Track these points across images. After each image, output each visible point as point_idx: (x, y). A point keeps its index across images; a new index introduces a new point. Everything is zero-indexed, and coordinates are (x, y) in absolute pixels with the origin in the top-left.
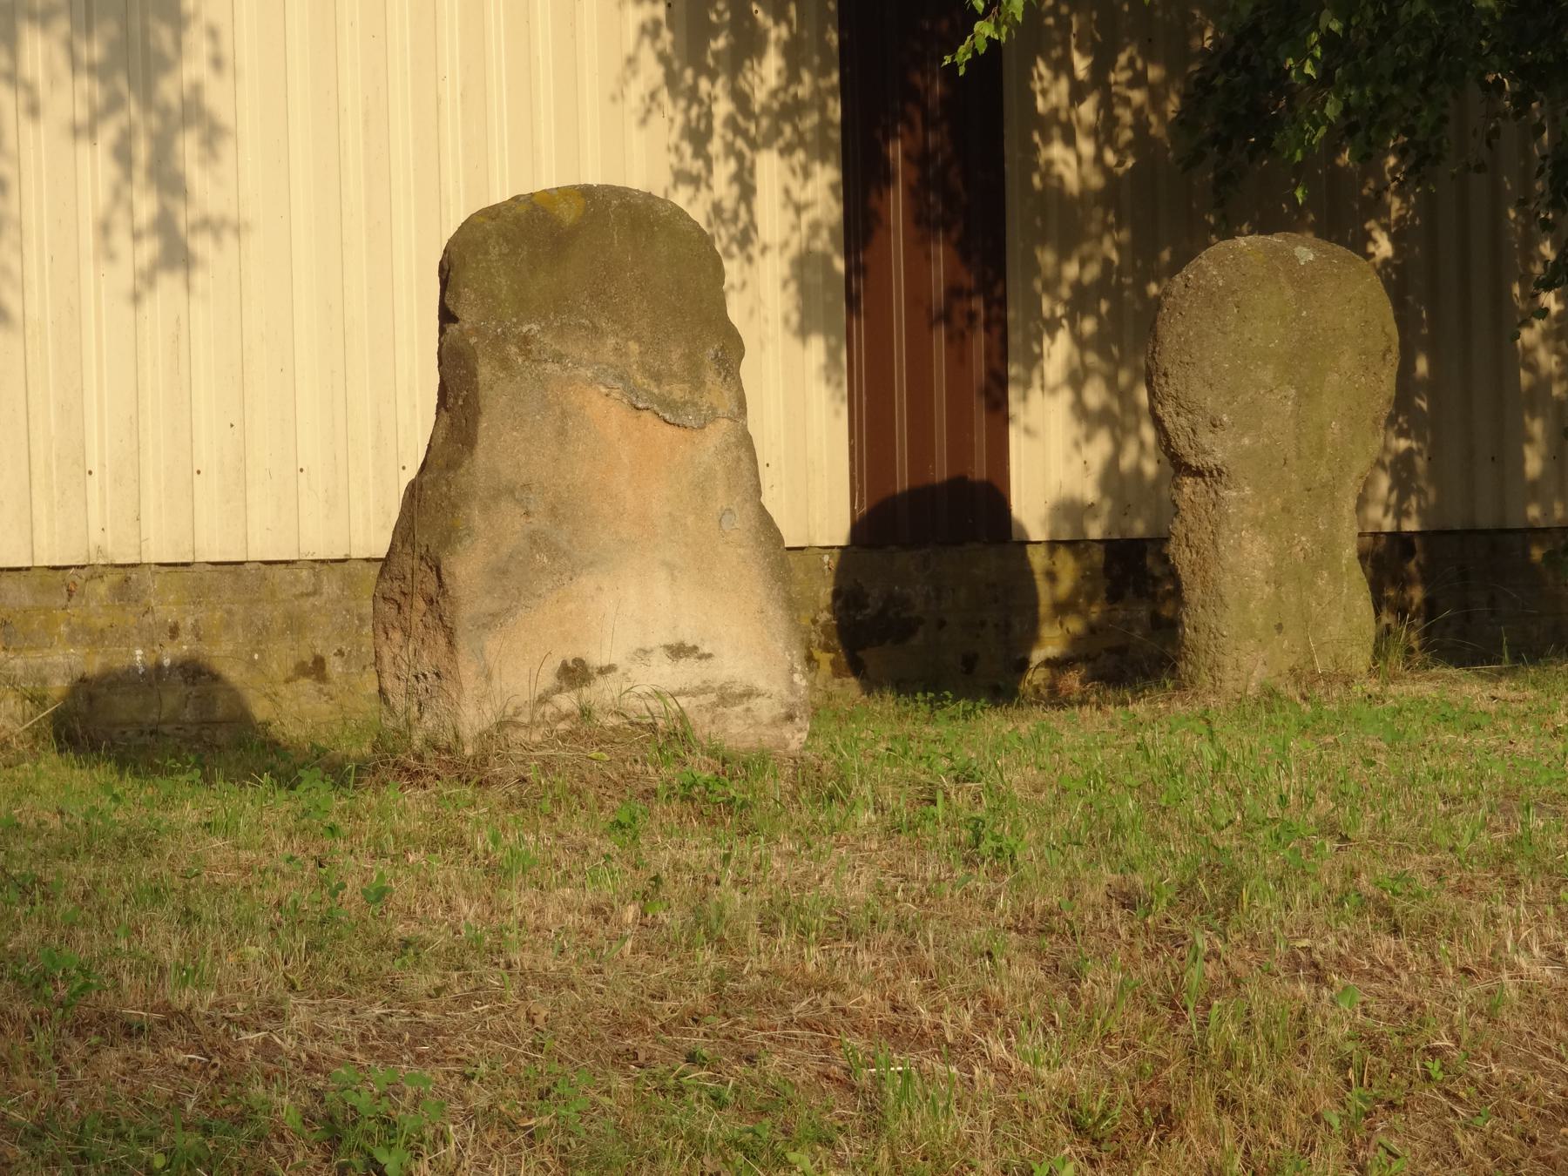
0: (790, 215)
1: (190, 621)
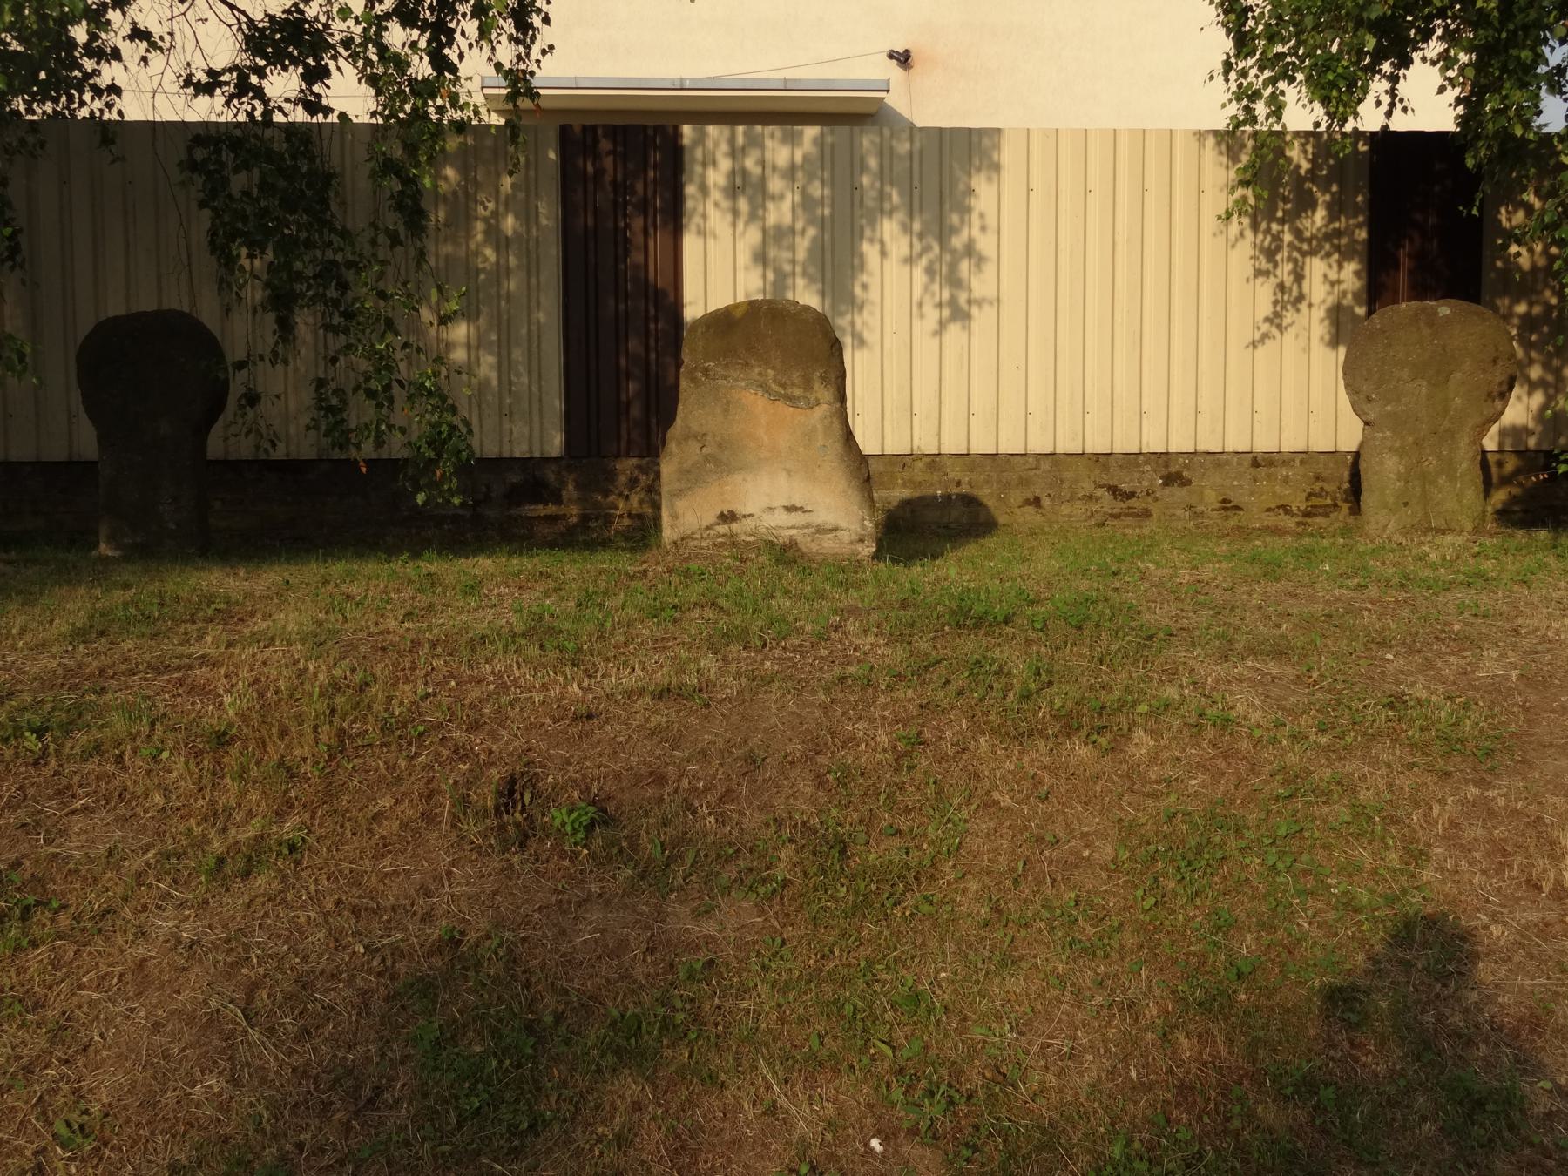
0: (1328, 287)
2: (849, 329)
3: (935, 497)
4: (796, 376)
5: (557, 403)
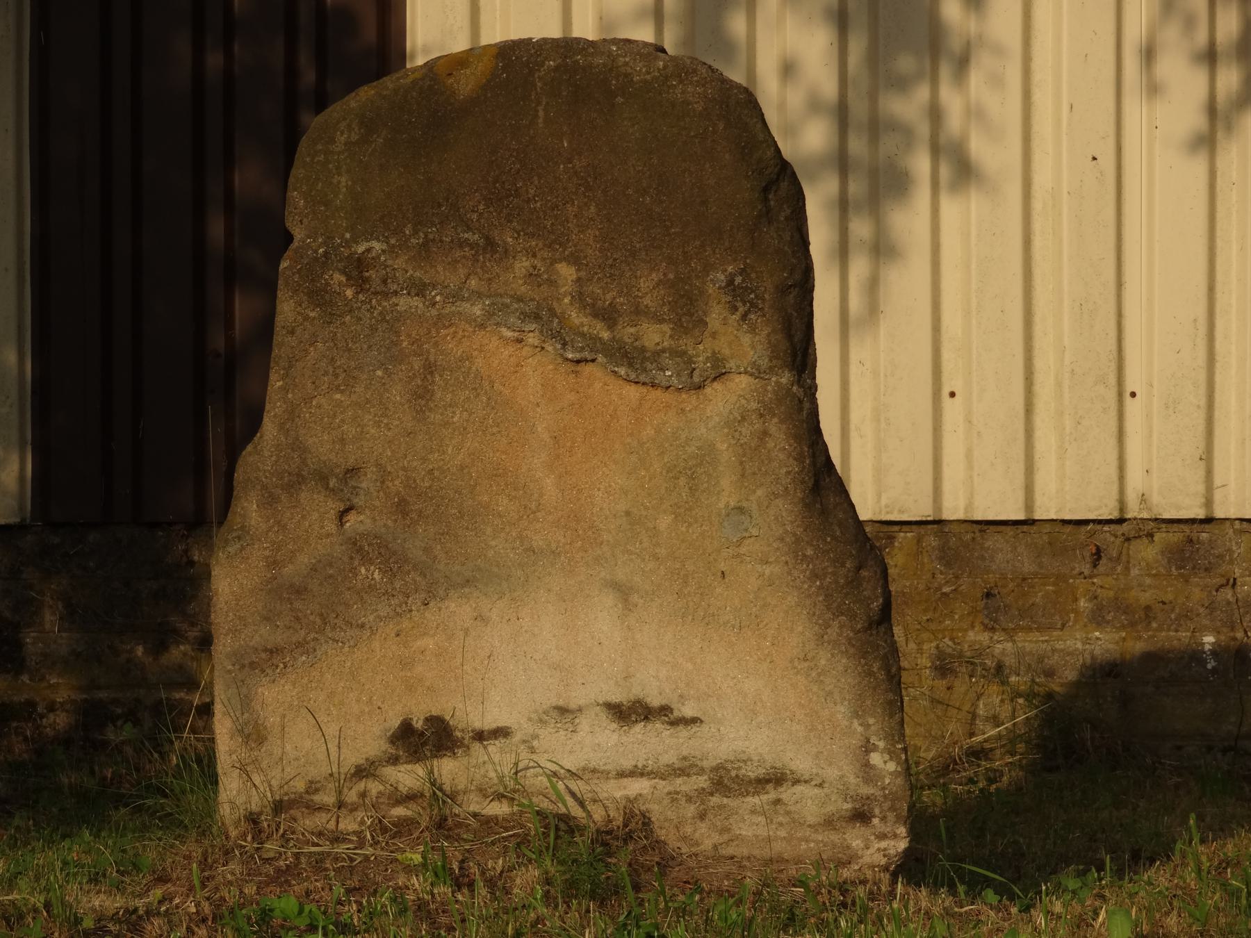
2: (923, 130)
3: (1196, 656)
4: (648, 286)
5: (11, 357)
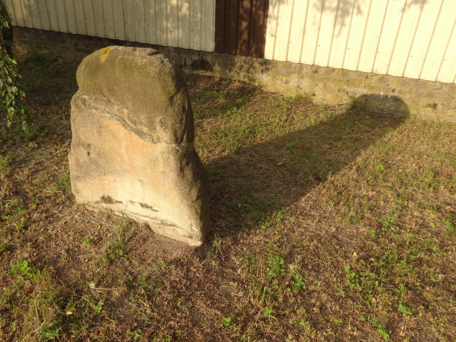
1: (399, 89)
3: (380, 96)
4: (143, 118)
5: (212, 28)
